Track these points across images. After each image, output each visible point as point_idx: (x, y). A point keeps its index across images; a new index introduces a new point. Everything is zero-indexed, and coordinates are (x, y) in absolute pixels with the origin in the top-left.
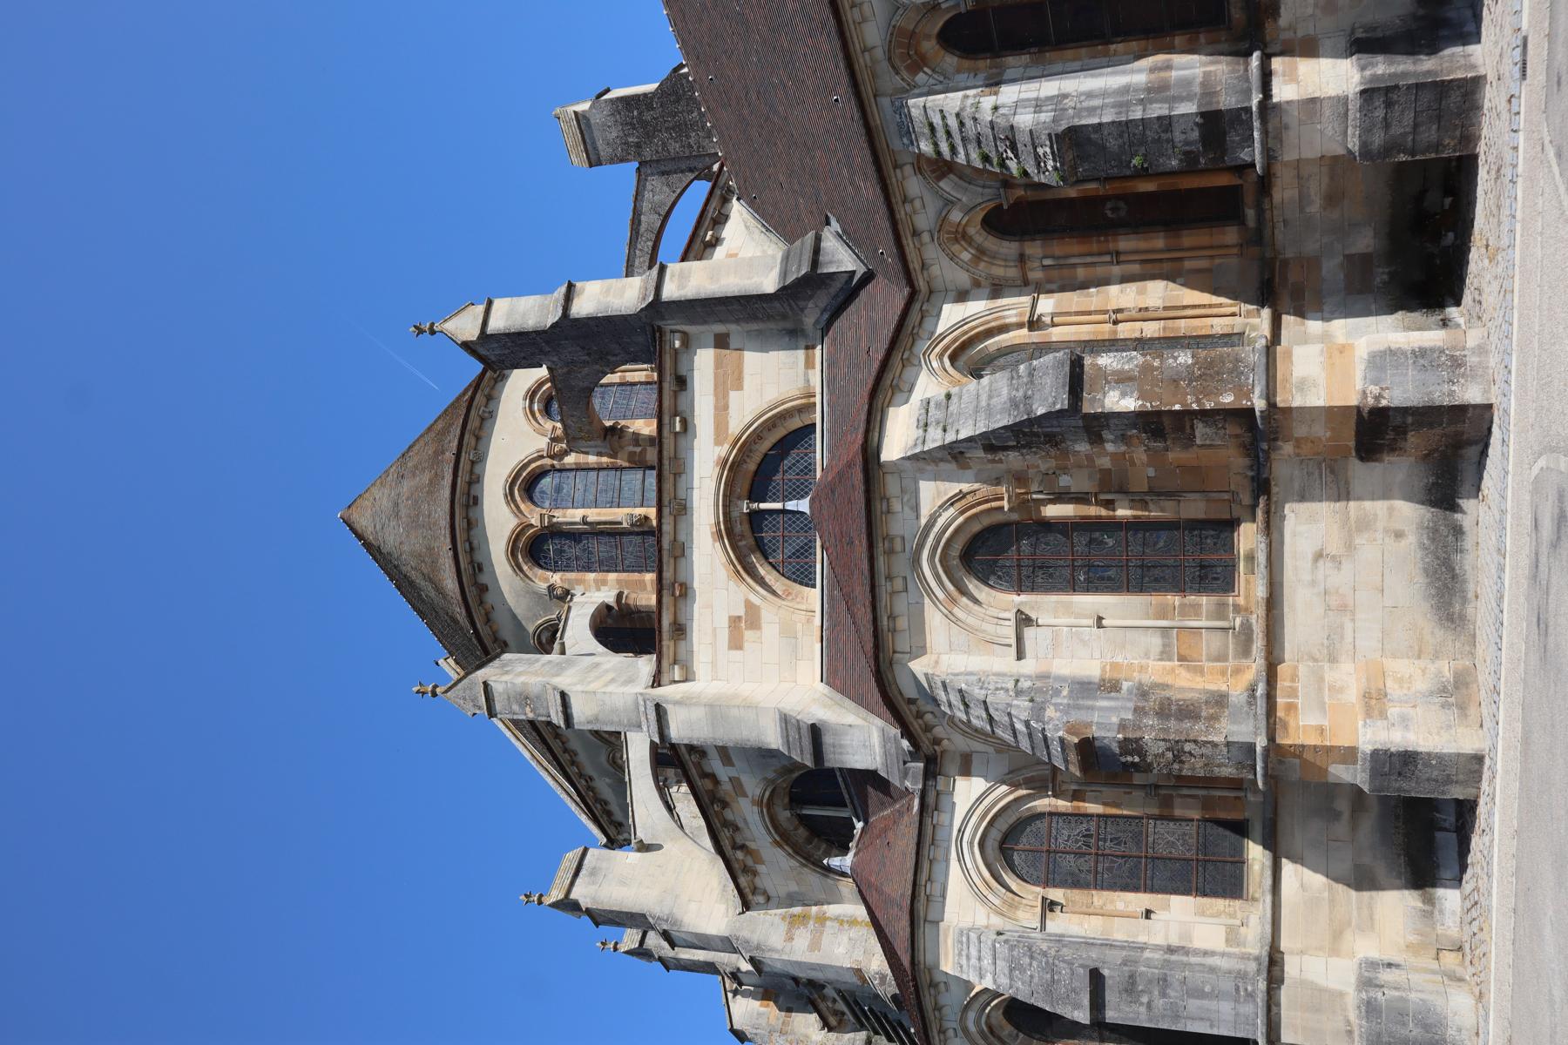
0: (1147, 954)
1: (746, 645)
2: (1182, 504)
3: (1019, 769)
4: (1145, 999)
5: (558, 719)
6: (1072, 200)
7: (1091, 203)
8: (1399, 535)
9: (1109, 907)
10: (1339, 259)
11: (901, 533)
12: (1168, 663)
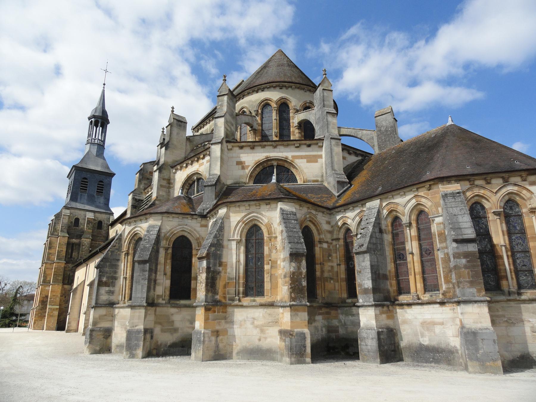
0: (154, 275)
5: (216, 115)
8: (260, 340)
10: (337, 324)
12: (227, 279)
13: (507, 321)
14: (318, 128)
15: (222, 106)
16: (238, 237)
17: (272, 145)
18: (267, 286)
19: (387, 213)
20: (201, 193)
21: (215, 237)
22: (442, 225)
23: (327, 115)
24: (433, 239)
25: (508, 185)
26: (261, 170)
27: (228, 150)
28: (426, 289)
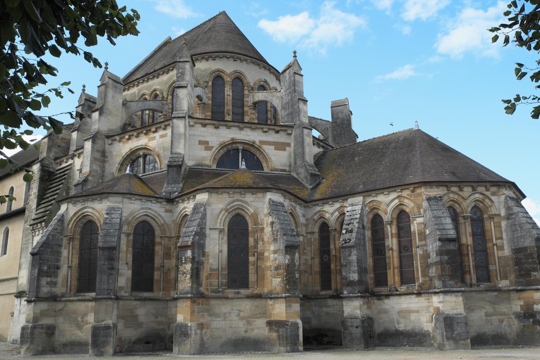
1: (200, 146)
2: (253, 275)
3: (168, 227)
4: (106, 263)
6: (329, 246)
7: (328, 252)
9: (128, 253)
10: (310, 316)
11: (246, 197)
13: (468, 308)
14: (286, 113)
15: (184, 74)
16: (221, 226)
17: (238, 126)
18: (252, 277)
19: (369, 210)
20: (155, 172)
21: (199, 225)
22: (422, 225)
23: (298, 101)
24: (413, 238)
25: (476, 193)
26: (225, 153)
27: (190, 126)
28: (402, 283)
